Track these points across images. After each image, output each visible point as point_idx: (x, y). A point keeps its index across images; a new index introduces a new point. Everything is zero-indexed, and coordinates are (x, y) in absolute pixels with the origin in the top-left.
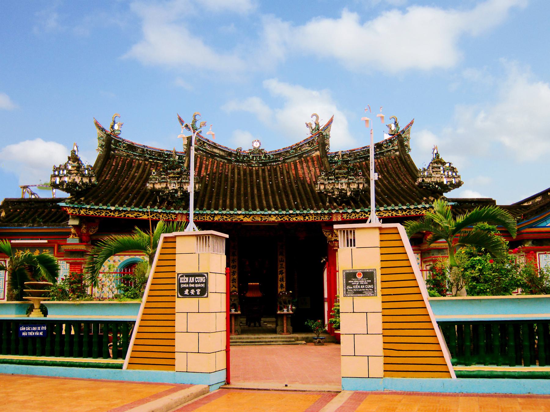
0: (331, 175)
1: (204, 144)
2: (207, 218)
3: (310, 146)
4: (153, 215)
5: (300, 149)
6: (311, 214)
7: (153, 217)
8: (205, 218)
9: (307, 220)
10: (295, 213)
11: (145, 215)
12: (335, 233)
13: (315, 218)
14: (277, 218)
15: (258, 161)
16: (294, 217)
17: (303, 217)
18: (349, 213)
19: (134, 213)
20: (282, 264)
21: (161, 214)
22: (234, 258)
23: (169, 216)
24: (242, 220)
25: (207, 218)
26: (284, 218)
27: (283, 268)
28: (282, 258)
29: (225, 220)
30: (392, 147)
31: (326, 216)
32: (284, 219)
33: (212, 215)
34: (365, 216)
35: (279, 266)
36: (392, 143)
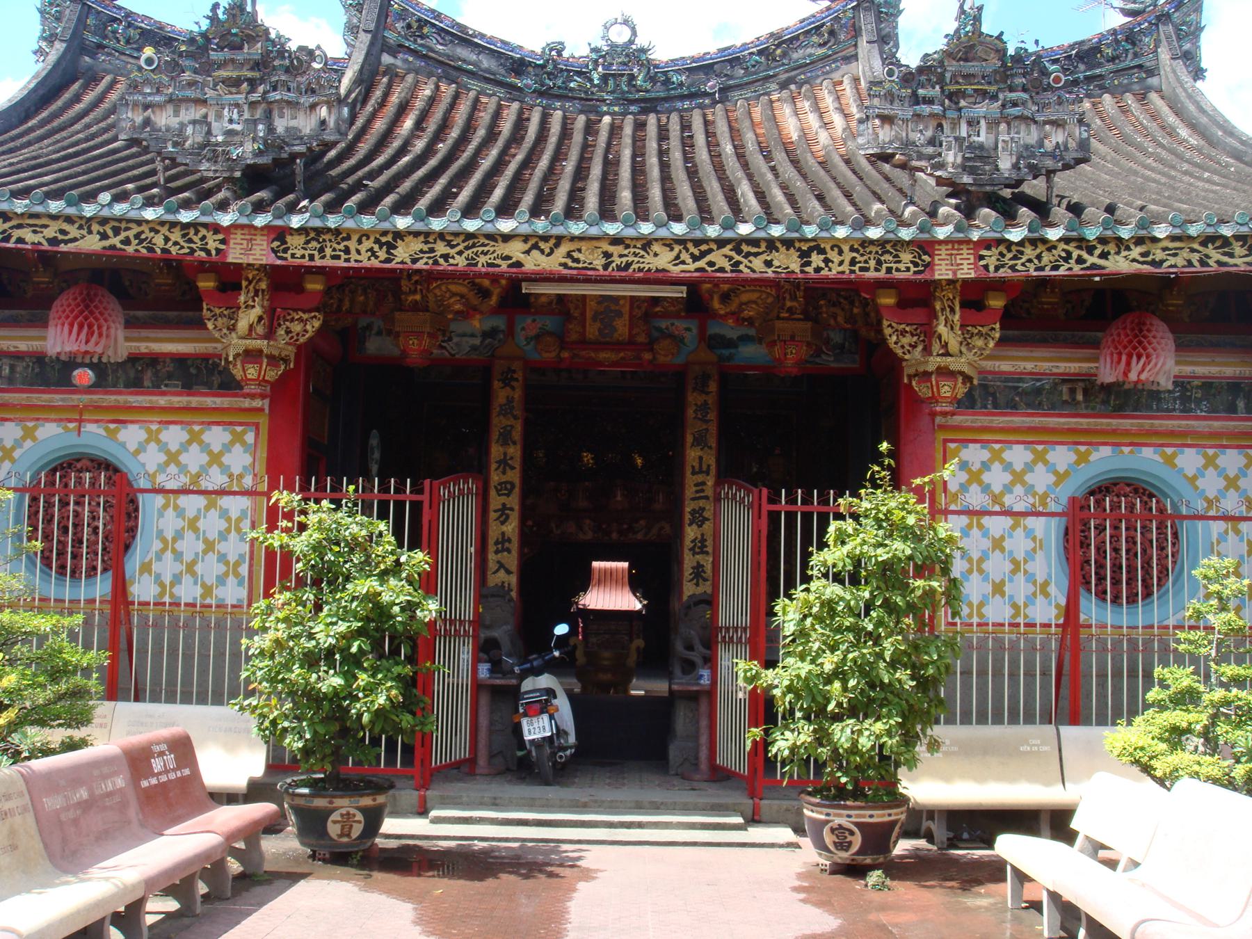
0: (929, 80)
1: (420, 28)
2: (358, 252)
3: (825, 44)
4: (123, 235)
5: (784, 55)
6: (837, 246)
7: (127, 242)
8: (353, 251)
9: (818, 270)
10: (762, 234)
11: (90, 232)
12: (940, 337)
13: (853, 262)
14: (678, 257)
15: (623, 93)
16: (756, 255)
17: (801, 257)
18: (1009, 244)
19: (46, 226)
20: (704, 483)
21: (157, 232)
22: (505, 454)
23: (196, 239)
24: (519, 264)
25: (358, 252)
26: (709, 258)
27: (707, 498)
28: (701, 458)
29: (441, 261)
30: (1136, 55)
31: (906, 257)
32: (711, 264)
33: (384, 239)
34: (1080, 260)
35: (690, 491)
36: (1134, 44)
